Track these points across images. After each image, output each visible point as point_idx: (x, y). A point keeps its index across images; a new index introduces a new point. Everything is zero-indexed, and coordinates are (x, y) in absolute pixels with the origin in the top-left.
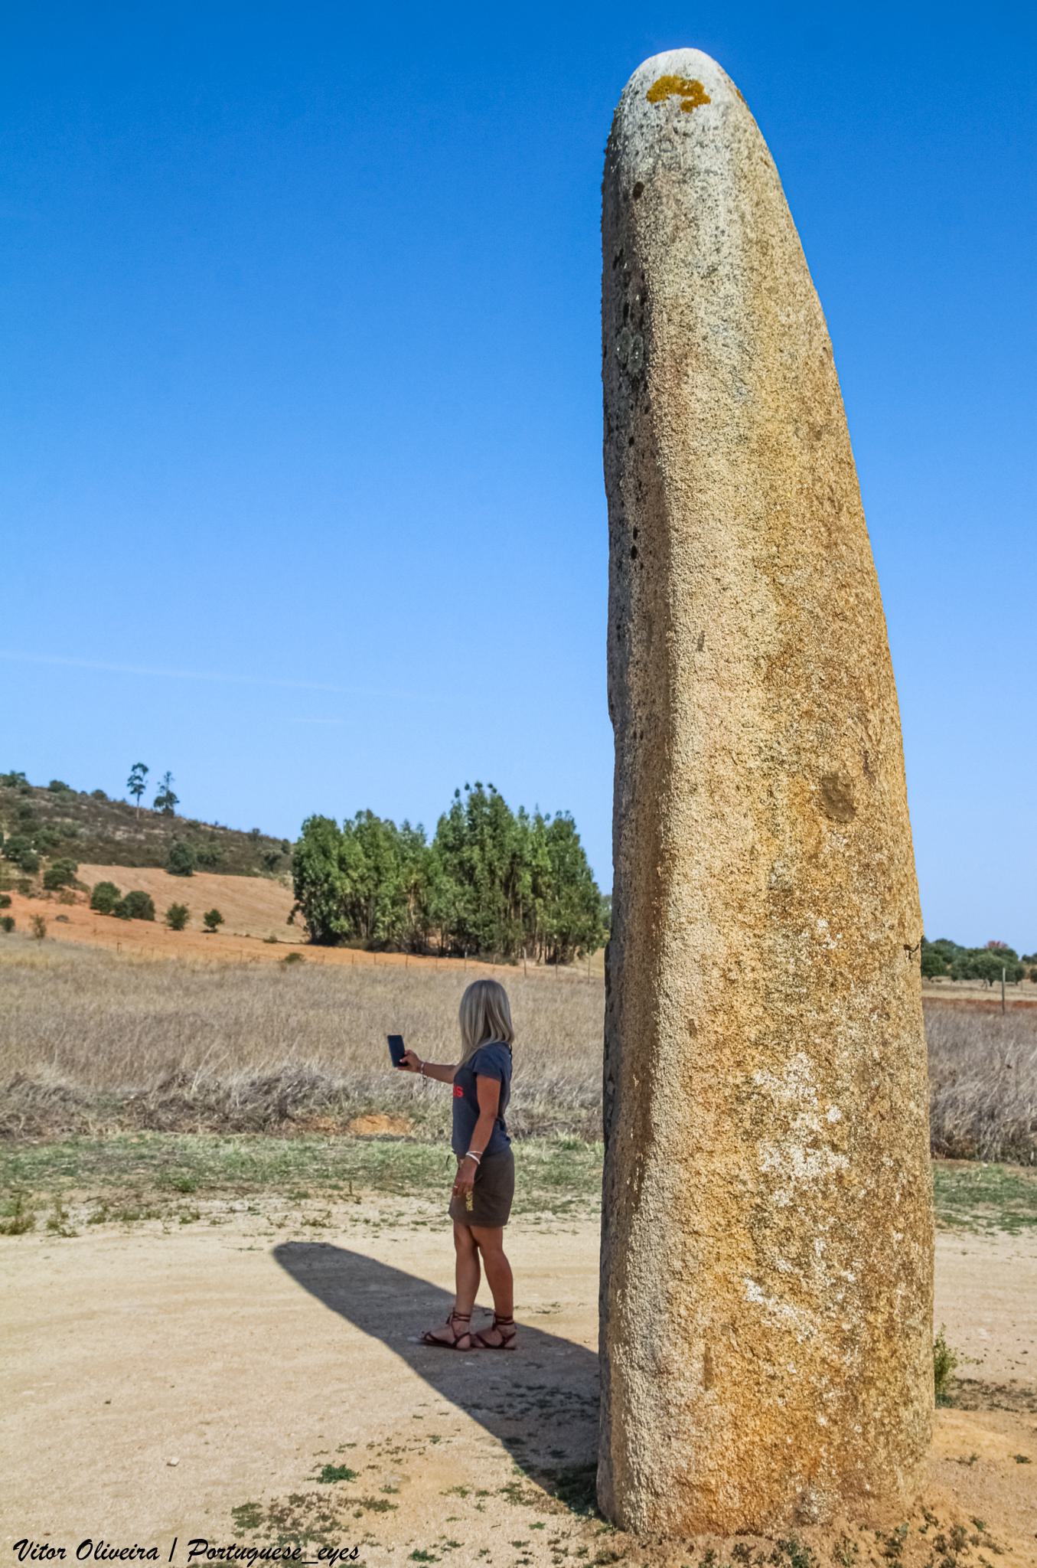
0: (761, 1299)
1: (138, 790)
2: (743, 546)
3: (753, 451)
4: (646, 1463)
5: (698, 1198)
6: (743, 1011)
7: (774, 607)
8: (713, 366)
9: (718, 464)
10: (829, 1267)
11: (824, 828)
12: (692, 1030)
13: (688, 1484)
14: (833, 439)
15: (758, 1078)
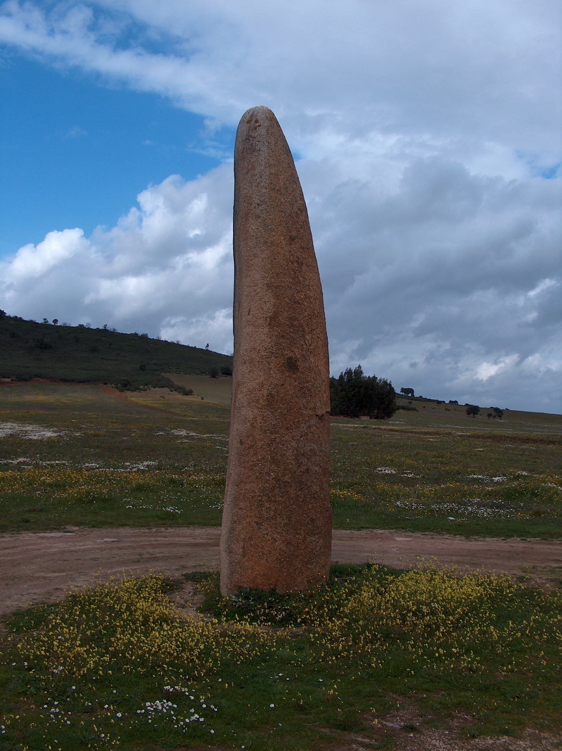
6: (257, 437)
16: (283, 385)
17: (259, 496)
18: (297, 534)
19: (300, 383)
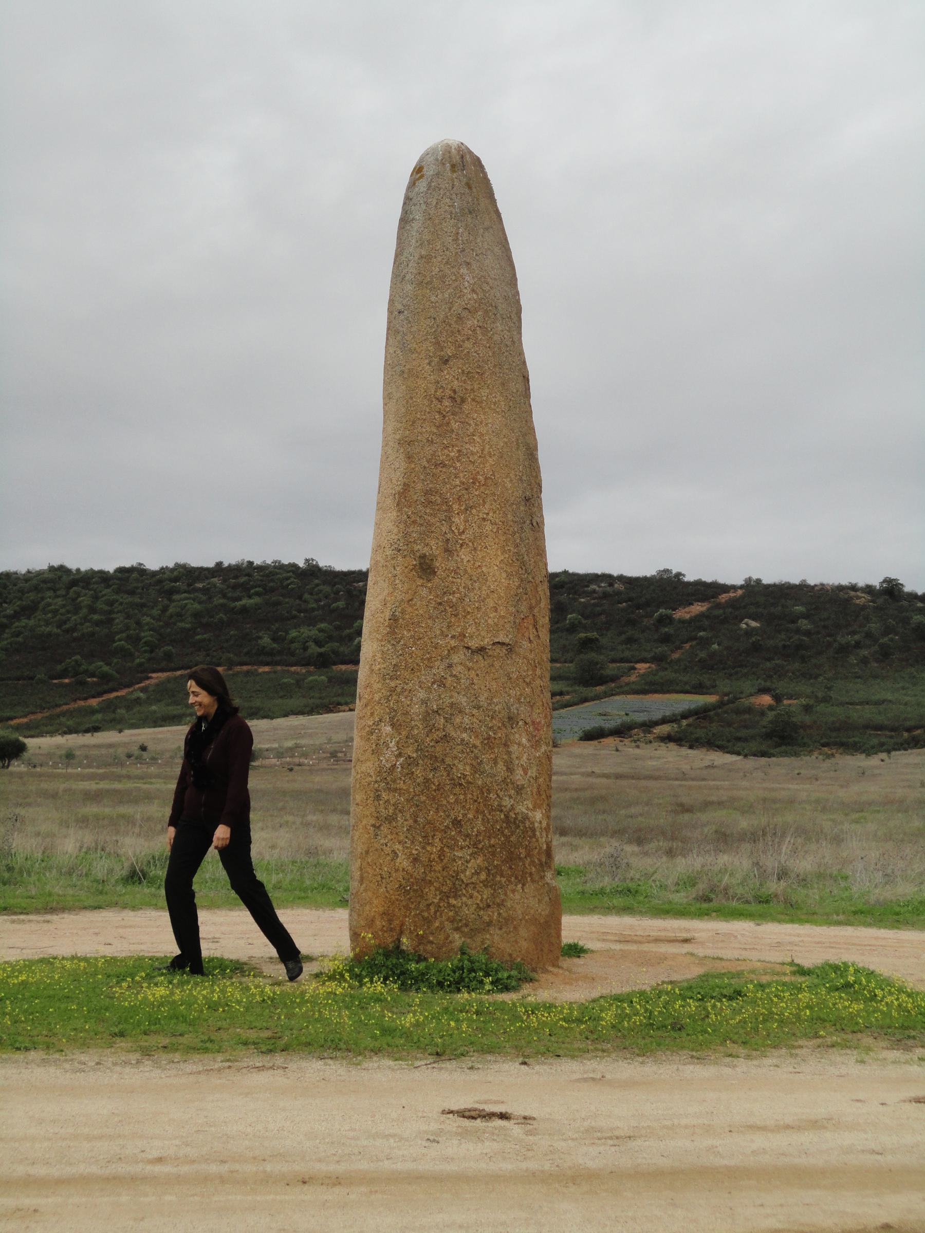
16: (411, 600)
17: (376, 782)
18: (429, 844)
19: (437, 596)
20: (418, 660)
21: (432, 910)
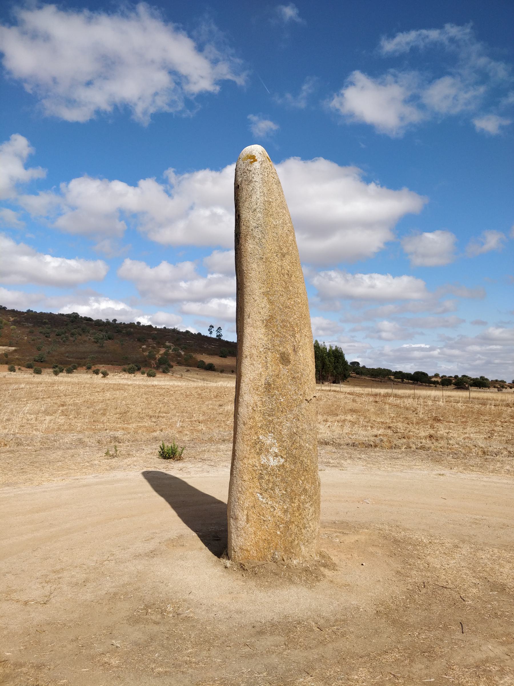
0: (261, 499)
1: (211, 333)
2: (260, 289)
3: (264, 262)
4: (233, 544)
5: (245, 471)
6: (257, 418)
7: (268, 306)
8: (254, 237)
9: (254, 266)
10: (280, 490)
11: (281, 367)
12: (244, 424)
13: (242, 549)
14: (289, 257)
15: (261, 437)
20: (285, 407)
21: (293, 536)
